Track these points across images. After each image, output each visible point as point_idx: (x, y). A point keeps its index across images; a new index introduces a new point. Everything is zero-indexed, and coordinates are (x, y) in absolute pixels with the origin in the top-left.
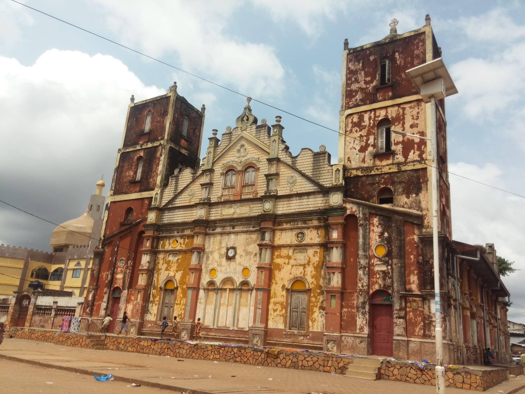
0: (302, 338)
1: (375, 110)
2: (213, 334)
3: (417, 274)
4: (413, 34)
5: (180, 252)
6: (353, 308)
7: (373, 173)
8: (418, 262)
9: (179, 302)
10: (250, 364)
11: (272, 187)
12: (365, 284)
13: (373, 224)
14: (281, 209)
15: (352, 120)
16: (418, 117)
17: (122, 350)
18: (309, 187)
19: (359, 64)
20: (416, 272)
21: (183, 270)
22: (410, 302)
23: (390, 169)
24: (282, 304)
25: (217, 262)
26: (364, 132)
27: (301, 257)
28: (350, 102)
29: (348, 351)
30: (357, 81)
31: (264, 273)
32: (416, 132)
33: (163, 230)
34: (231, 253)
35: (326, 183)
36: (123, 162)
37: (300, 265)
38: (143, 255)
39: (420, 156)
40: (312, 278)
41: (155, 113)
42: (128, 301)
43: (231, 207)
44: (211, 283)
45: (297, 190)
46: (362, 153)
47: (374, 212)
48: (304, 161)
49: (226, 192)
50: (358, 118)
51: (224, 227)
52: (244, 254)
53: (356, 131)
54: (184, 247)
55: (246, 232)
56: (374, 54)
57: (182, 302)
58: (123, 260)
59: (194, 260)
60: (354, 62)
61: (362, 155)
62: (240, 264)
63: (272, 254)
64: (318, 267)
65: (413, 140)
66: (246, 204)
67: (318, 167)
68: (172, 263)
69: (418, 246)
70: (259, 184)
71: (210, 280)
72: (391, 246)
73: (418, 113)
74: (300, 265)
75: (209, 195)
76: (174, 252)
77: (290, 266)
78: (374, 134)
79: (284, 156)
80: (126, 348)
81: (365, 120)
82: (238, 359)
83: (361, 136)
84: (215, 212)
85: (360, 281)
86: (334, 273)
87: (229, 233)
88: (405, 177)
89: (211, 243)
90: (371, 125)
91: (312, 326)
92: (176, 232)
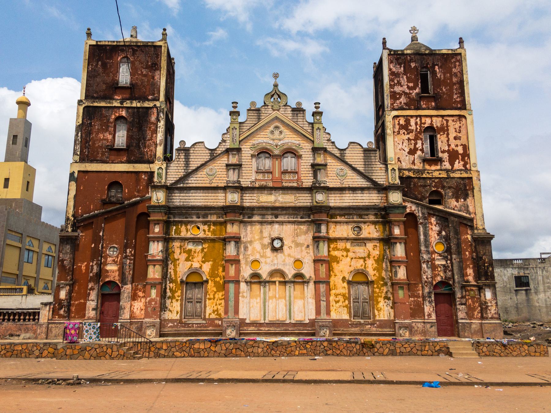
0: (369, 326)
1: (420, 116)
2: (267, 329)
3: (473, 268)
4: (450, 52)
5: (204, 240)
6: (419, 297)
7: (424, 176)
8: (472, 258)
9: (212, 297)
10: (344, 355)
11: (320, 177)
12: (429, 276)
13: (431, 223)
14: (332, 201)
15: (399, 122)
16: (460, 130)
17: (165, 356)
18: (361, 182)
19: (401, 67)
20: (471, 266)
21: (212, 261)
22: (468, 291)
23: (440, 174)
24: (344, 295)
25: (260, 253)
26: (411, 136)
27: (360, 251)
28: (394, 103)
29: (419, 335)
30: (399, 84)
31: (324, 265)
32: (459, 144)
33: (173, 215)
34: (277, 244)
35: (380, 180)
36: (90, 119)
37: (360, 258)
38: (151, 244)
39: (465, 165)
40: (374, 270)
41: (137, 63)
42: (134, 297)
43: (271, 194)
44: (255, 275)
45: (349, 183)
46: (411, 156)
47: (432, 212)
48: (354, 155)
49: (260, 177)
50: (405, 121)
51: (263, 215)
52: (293, 246)
53: (404, 133)
54: (209, 235)
55: (294, 222)
56: (415, 61)
57: (216, 296)
58: (114, 247)
59: (231, 250)
60: (396, 64)
61: (412, 157)
62: (289, 255)
63: (329, 247)
64: (380, 261)
65: (457, 151)
66: (290, 192)
67: (370, 163)
68: (195, 252)
69: (471, 245)
70: (302, 172)
71: (252, 272)
72: (449, 243)
73: (460, 127)
74: (360, 258)
75: (239, 178)
76: (195, 240)
77: (348, 259)
78: (421, 139)
79: (330, 147)
80: (171, 354)
81: (411, 124)
82: (329, 352)
83: (409, 139)
84: (250, 198)
85: (424, 273)
86: (399, 267)
87: (272, 223)
88: (453, 183)
89: (248, 232)
90: (418, 130)
91: (379, 315)
92: (195, 217)
